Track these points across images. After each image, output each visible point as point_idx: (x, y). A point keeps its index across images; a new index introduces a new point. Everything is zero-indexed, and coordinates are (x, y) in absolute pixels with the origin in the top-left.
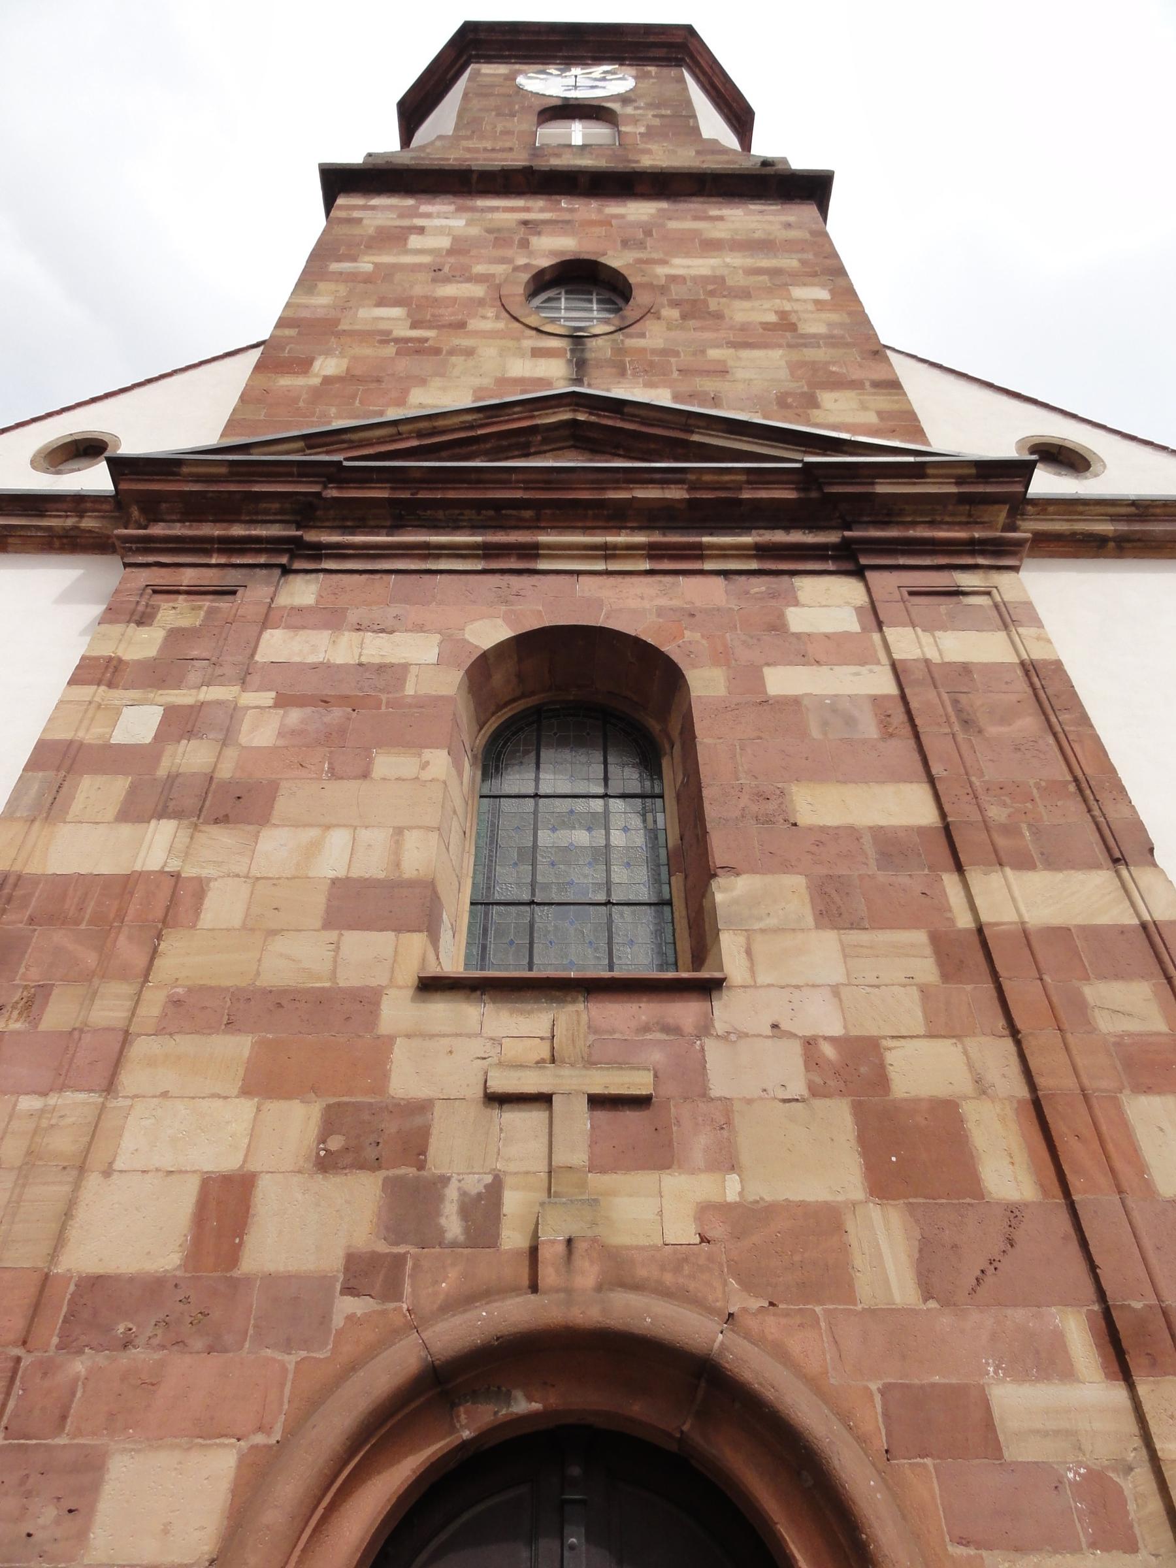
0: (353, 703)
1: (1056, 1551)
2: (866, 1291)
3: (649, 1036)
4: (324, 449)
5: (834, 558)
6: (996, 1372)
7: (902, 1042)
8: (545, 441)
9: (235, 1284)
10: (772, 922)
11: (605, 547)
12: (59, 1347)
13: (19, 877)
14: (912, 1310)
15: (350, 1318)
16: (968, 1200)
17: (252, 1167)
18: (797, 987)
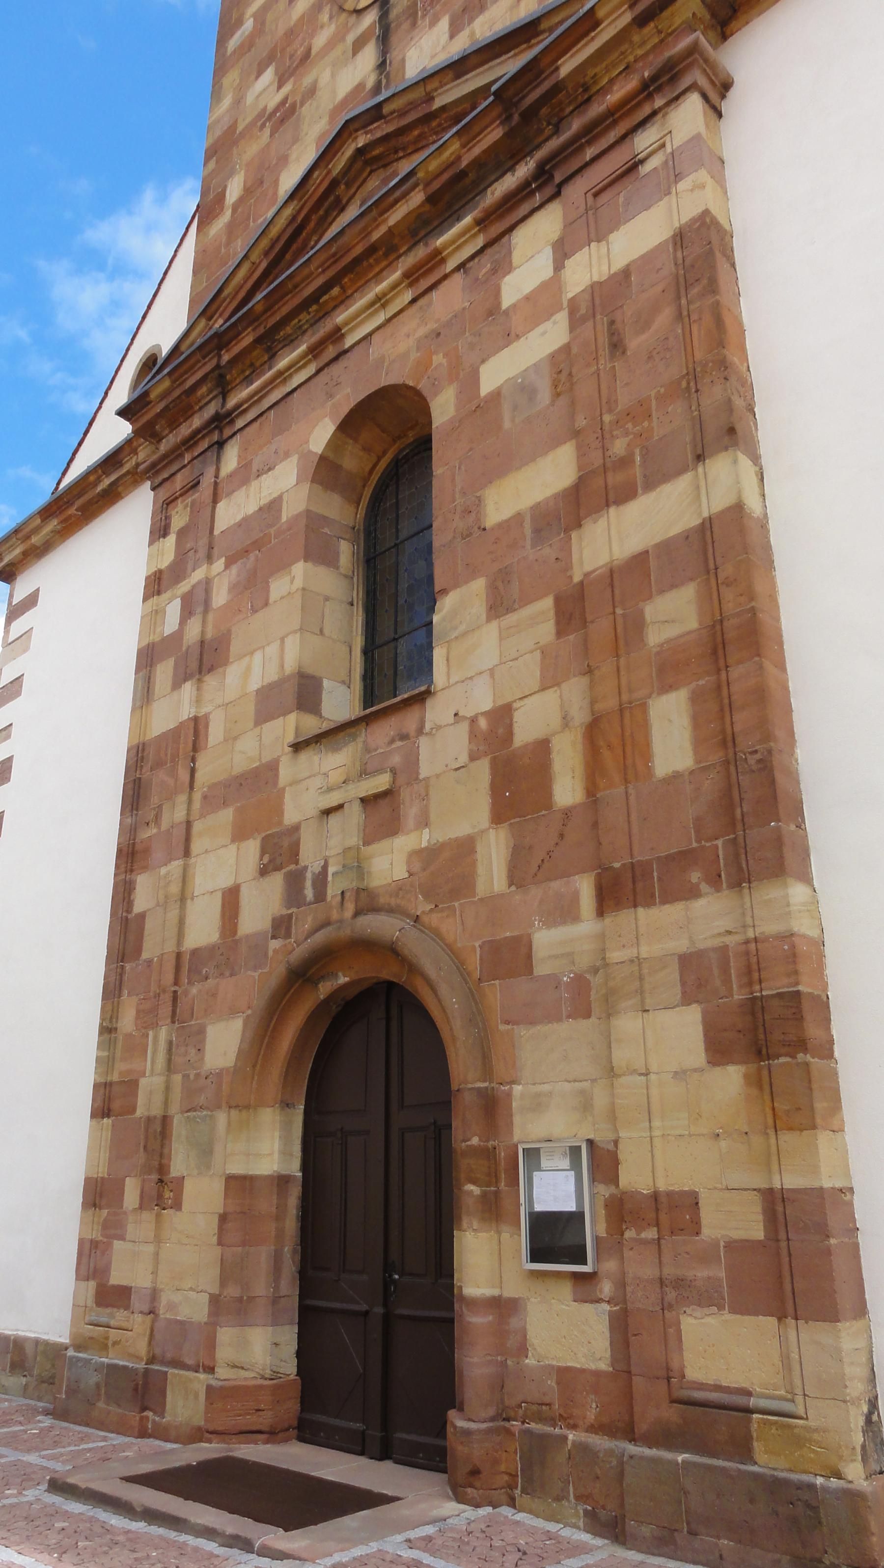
0: (257, 545)
1: (549, 1022)
2: (481, 889)
3: (394, 746)
4: (217, 315)
5: (539, 188)
6: (539, 924)
7: (526, 701)
8: (348, 185)
9: (236, 942)
10: (462, 628)
11: (378, 298)
12: (189, 983)
13: (144, 744)
14: (502, 894)
15: (275, 951)
16: (544, 812)
17: (238, 882)
18: (471, 678)
